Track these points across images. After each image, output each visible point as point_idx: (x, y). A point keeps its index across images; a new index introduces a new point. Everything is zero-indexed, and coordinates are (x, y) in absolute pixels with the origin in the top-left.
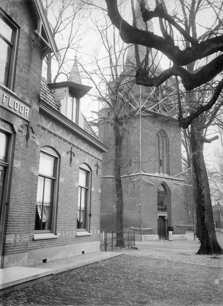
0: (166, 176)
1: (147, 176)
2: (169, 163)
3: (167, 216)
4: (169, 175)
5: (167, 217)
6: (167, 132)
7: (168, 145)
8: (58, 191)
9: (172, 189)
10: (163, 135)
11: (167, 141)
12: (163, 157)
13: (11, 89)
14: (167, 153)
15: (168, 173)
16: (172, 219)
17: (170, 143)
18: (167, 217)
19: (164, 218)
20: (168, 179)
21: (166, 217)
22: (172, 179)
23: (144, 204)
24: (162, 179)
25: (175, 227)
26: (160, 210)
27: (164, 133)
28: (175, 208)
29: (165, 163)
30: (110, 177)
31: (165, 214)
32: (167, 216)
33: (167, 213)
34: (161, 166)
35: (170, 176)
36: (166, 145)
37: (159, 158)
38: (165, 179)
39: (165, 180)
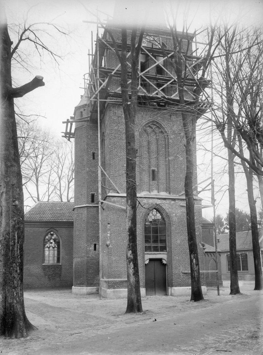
0: (164, 194)
1: (121, 198)
2: (169, 173)
3: (166, 259)
4: (170, 193)
5: (167, 260)
6: (164, 124)
7: (167, 146)
8: (163, 254)
9: (174, 215)
10: (157, 130)
11: (167, 138)
12: (158, 166)
13: (112, 71)
14: (166, 158)
15: (168, 190)
16: (174, 262)
17: (170, 141)
18: (167, 260)
19: (162, 262)
20: (159, 199)
21: (163, 259)
22: (174, 200)
23: (113, 241)
24: (151, 201)
25: (181, 274)
26: (152, 249)
27: (160, 127)
28: (180, 245)
29: (162, 175)
30: (84, 207)
31: (162, 255)
32: (166, 259)
33: (166, 253)
34: (154, 179)
35: (171, 194)
36: (164, 146)
37: (149, 167)
38: (159, 201)
39: (159, 202)
